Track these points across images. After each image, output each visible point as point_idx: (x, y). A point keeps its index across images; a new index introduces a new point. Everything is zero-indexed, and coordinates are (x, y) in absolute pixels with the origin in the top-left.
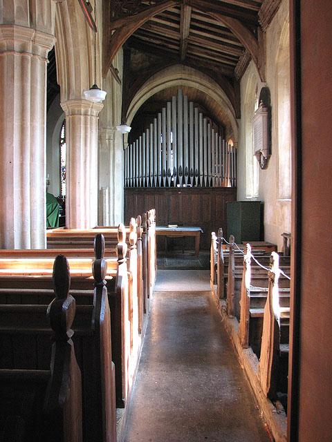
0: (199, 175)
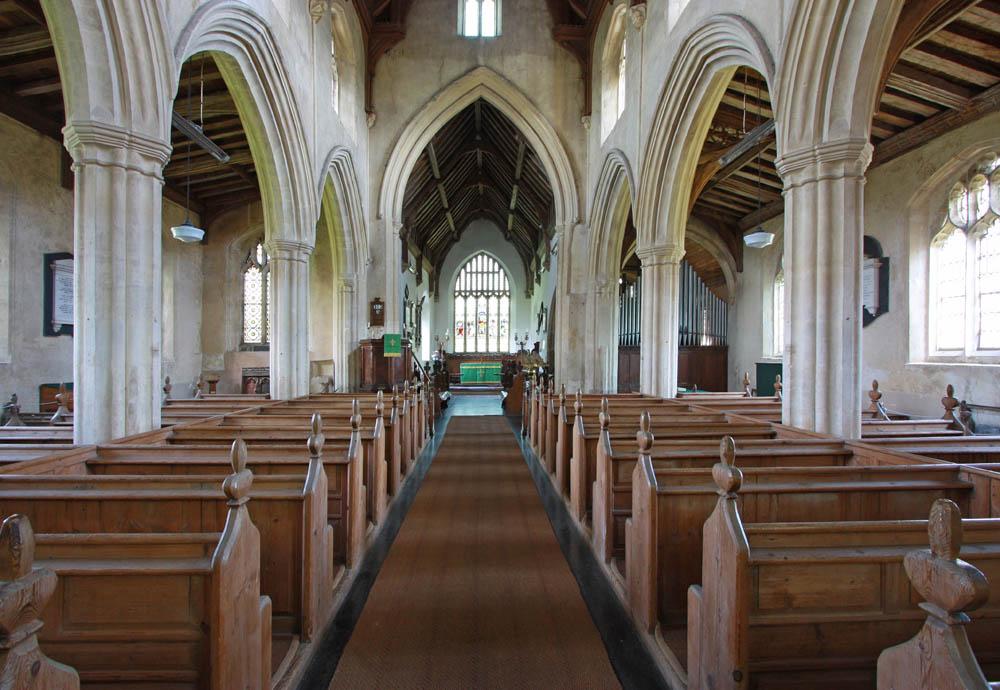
0: (687, 333)
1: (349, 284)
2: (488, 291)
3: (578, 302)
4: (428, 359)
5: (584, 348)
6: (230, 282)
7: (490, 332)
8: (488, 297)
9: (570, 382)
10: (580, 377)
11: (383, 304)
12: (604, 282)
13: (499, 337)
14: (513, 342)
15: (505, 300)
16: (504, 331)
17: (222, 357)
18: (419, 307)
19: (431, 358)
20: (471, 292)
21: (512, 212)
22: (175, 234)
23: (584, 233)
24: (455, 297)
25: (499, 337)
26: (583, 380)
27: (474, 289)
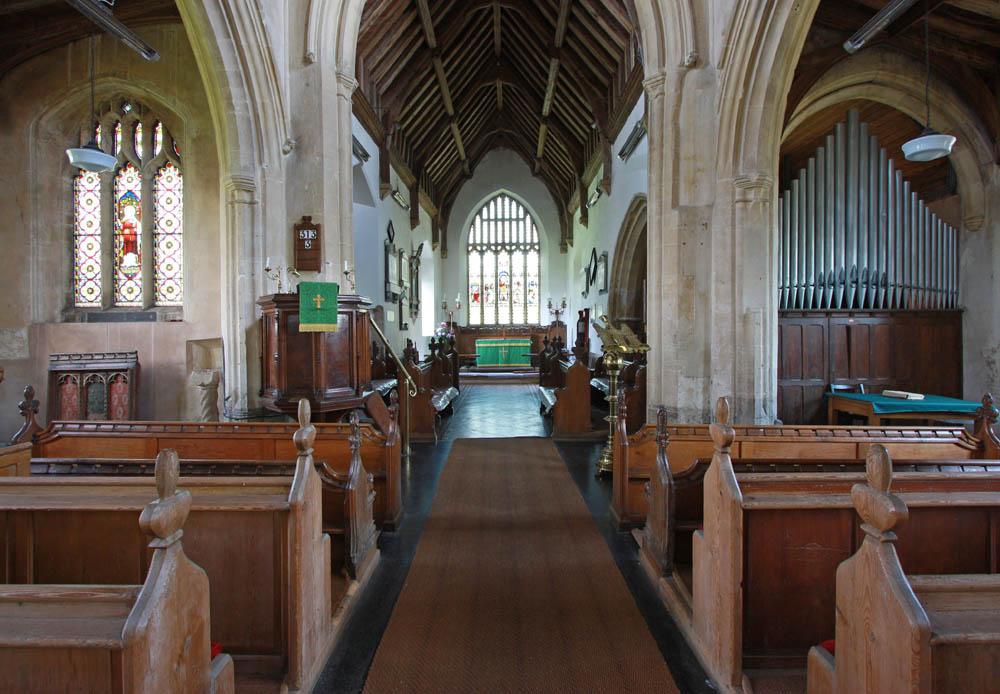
0: (885, 285)
1: (245, 186)
2: (511, 244)
3: (694, 222)
4: (432, 334)
5: (707, 313)
6: (37, 190)
7: (514, 298)
8: (510, 252)
9: (682, 379)
10: (701, 369)
11: (317, 228)
12: (754, 177)
13: (526, 304)
14: (546, 311)
15: (533, 256)
16: (533, 297)
17: (24, 333)
18: (415, 260)
19: (436, 334)
20: (489, 245)
21: (545, 120)
22: (71, 159)
23: (707, 83)
24: (468, 252)
25: (526, 304)
26: (708, 376)
27: (493, 241)
